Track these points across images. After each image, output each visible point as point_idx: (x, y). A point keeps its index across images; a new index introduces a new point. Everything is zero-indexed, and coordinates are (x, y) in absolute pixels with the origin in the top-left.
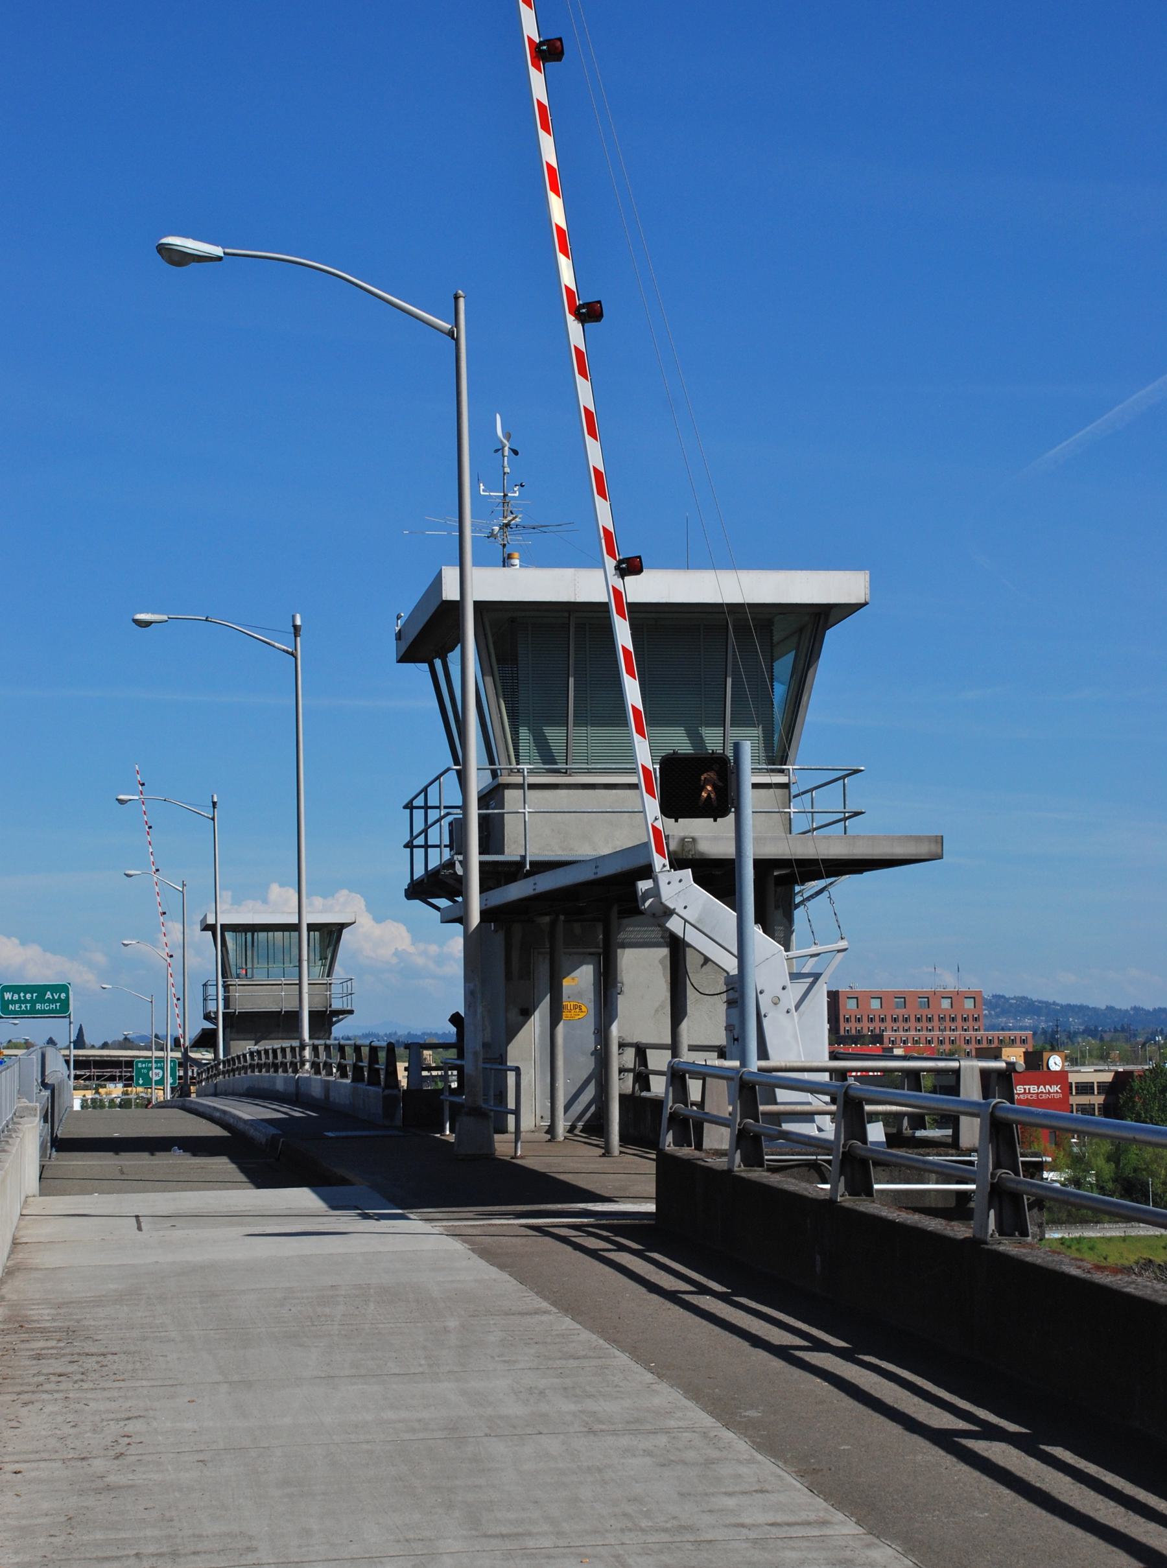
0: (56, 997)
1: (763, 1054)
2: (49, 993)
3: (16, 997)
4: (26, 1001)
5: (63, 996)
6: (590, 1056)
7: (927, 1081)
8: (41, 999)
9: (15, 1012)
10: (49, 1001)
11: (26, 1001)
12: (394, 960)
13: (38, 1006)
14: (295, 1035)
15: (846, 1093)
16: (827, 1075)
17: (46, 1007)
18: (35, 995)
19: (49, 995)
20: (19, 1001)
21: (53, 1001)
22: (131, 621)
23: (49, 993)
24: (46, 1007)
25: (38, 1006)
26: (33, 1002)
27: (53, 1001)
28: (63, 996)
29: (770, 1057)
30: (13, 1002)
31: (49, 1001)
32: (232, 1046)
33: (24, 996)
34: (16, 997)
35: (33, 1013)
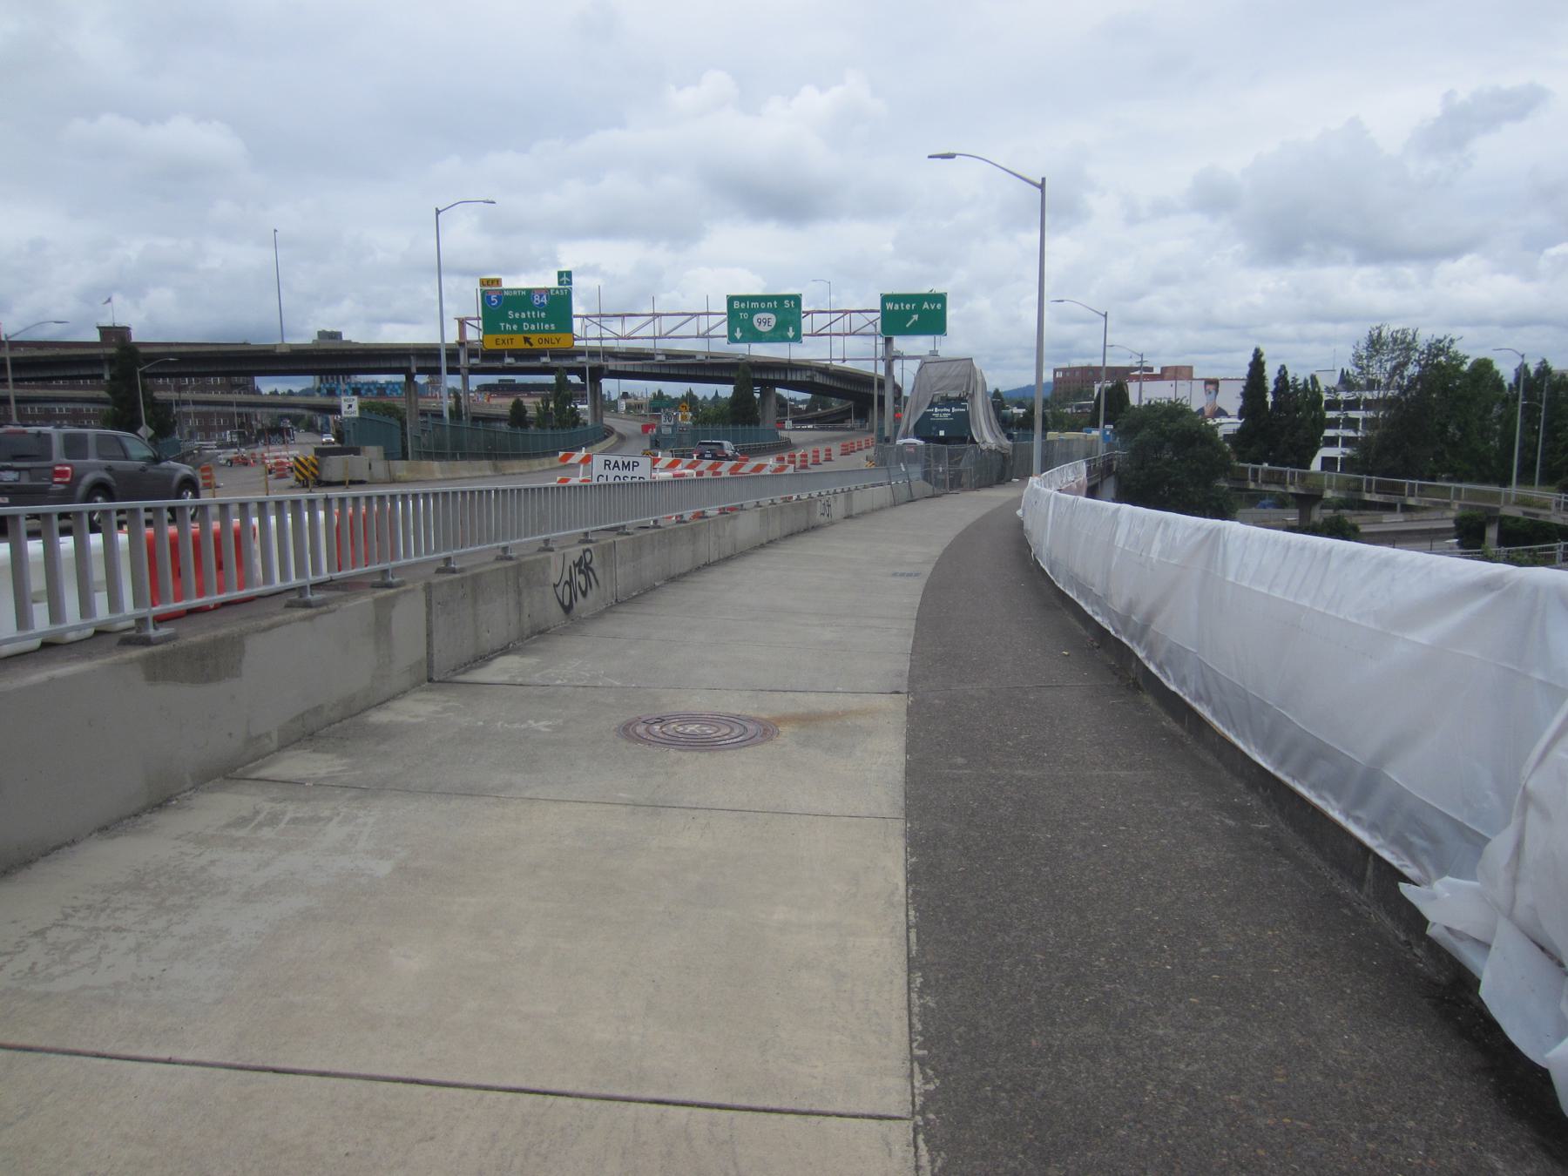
0: (933, 308)
18: (913, 305)
33: (904, 307)
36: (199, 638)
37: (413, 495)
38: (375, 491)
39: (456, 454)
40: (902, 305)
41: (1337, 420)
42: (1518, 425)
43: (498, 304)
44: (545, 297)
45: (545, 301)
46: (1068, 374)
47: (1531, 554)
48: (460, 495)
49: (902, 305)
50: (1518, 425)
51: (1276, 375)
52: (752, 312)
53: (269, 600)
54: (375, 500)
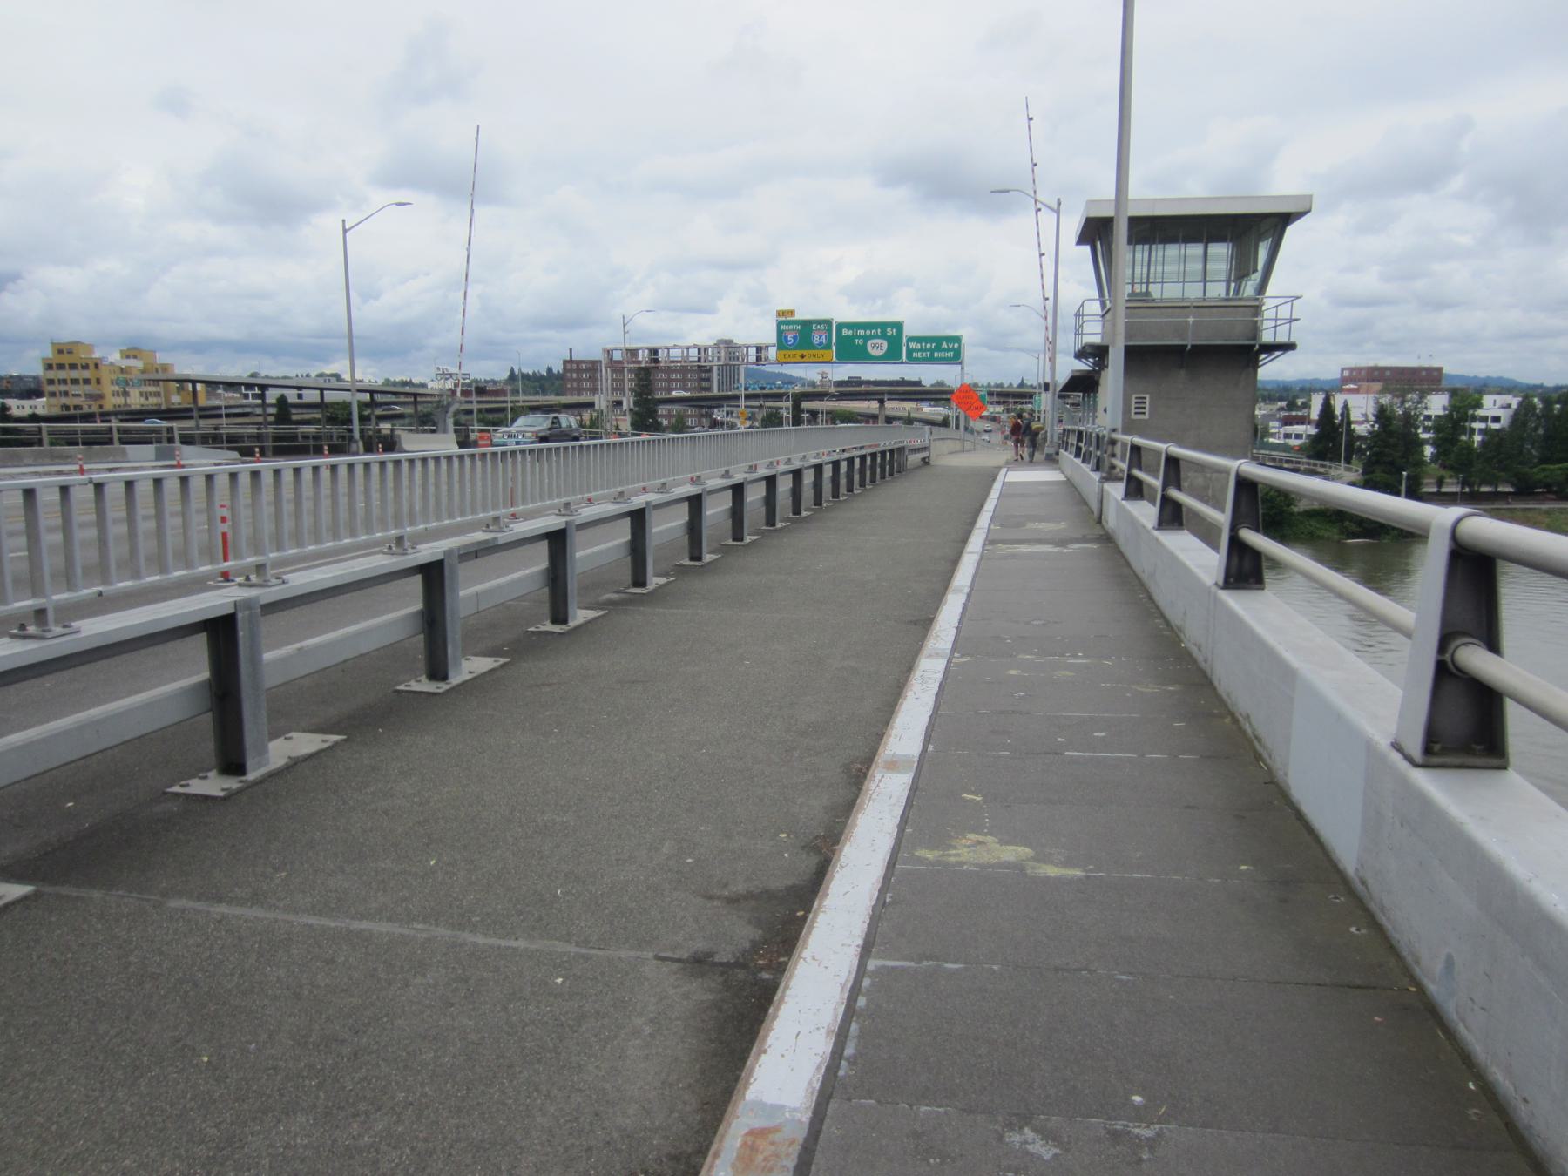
1: (888, 400)
2: (945, 343)
3: (919, 346)
4: (926, 350)
5: (956, 346)
6: (1128, 247)
7: (484, 411)
8: (938, 349)
9: (917, 359)
10: (945, 350)
11: (926, 350)
12: (811, 854)
13: (936, 354)
14: (93, 419)
15: (1131, 442)
16: (294, 418)
17: (941, 355)
18: (934, 345)
19: (944, 345)
20: (921, 350)
21: (948, 350)
22: (1057, 198)
23: (945, 343)
24: (941, 355)
25: (936, 354)
26: (932, 351)
27: (948, 350)
28: (956, 346)
29: (1311, 193)
30: (916, 350)
31: (945, 350)
32: (201, 635)
33: (926, 346)
34: (919, 346)
35: (931, 359)
36: (1025, 550)
37: (538, 450)
38: (585, 443)
39: (322, 446)
40: (923, 344)
41: (1456, 494)
42: (595, 549)
43: (795, 342)
44: (824, 337)
45: (824, 341)
46: (1354, 373)
47: (468, 1030)
48: (562, 451)
49: (923, 344)
50: (595, 549)
51: (1342, 405)
52: (866, 338)
53: (665, 510)
54: (605, 446)
